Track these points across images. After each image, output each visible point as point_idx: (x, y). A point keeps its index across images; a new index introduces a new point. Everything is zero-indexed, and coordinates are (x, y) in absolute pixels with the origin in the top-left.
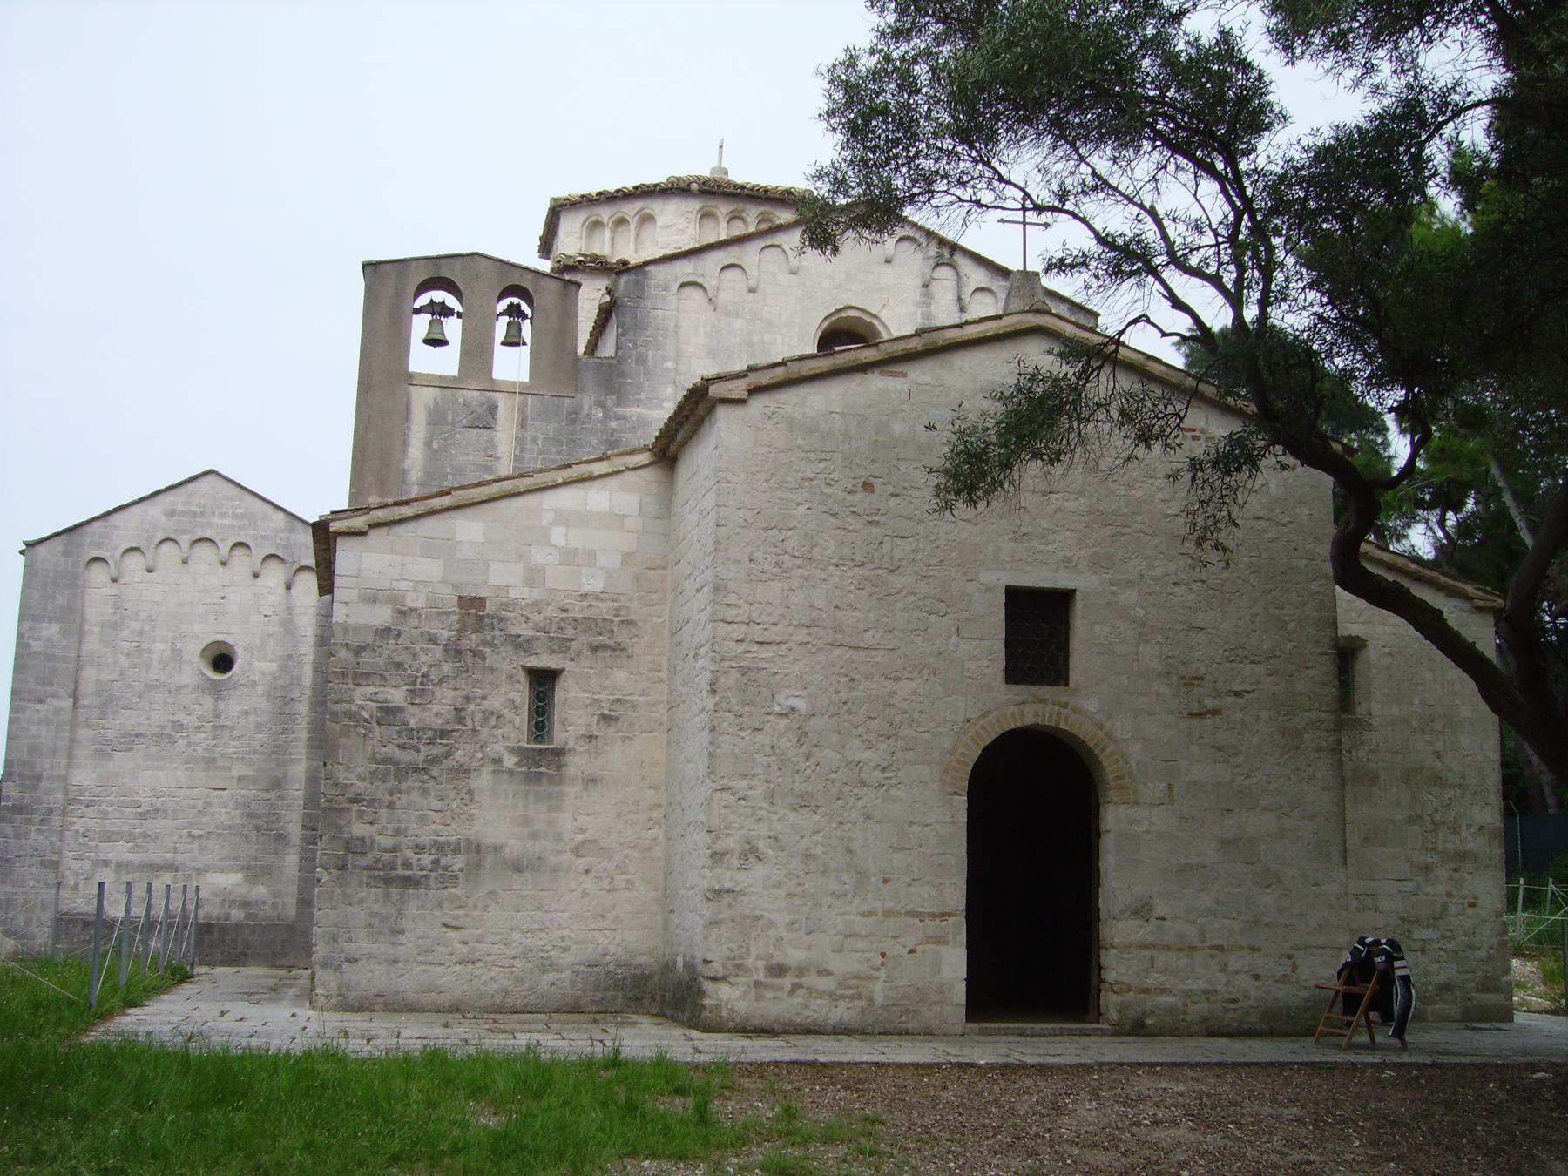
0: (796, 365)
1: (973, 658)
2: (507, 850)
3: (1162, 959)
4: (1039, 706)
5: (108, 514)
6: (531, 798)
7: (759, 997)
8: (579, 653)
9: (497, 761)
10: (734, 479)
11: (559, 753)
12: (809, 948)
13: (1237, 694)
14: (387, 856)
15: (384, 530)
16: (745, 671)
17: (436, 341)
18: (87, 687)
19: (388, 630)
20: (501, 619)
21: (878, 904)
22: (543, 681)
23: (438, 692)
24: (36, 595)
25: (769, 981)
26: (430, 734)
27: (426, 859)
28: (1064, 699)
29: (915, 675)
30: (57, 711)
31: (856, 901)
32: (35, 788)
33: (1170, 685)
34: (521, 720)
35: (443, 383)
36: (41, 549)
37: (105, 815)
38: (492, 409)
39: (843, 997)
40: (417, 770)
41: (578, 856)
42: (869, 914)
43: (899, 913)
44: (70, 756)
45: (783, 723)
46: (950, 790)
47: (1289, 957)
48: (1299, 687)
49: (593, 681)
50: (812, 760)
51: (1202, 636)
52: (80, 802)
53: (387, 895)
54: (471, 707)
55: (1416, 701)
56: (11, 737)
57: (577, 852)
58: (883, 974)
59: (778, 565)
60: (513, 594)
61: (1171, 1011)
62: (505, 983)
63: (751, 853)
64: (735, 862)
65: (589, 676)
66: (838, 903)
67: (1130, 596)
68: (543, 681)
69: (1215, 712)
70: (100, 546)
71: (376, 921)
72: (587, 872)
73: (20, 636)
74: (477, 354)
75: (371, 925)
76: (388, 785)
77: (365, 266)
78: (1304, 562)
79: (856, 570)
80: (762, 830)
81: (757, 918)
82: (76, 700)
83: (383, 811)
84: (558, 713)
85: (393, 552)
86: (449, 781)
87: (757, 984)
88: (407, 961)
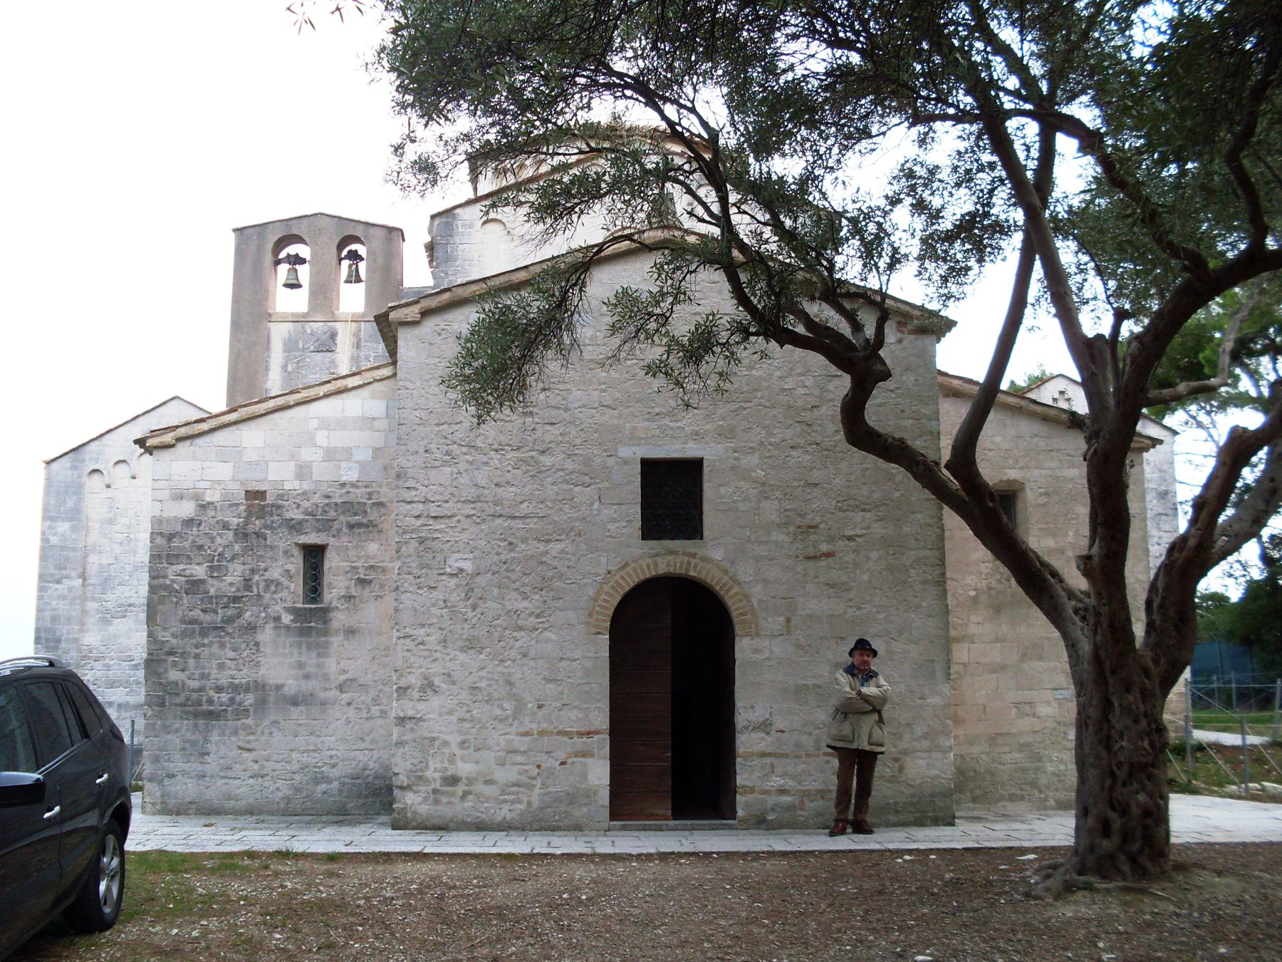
0: (460, 290)
1: (613, 520)
2: (286, 689)
3: (780, 765)
4: (671, 558)
5: (102, 435)
6: (304, 647)
7: (437, 802)
8: (340, 530)
9: (277, 619)
10: (411, 386)
11: (326, 611)
12: (477, 762)
13: (850, 538)
14: (195, 695)
15: (188, 443)
16: (422, 541)
17: (294, 285)
18: (92, 569)
19: (192, 520)
20: (279, 507)
21: (534, 726)
22: (314, 556)
23: (231, 567)
24: (53, 502)
25: (444, 789)
26: (225, 600)
27: (225, 697)
28: (692, 550)
29: (563, 537)
30: (70, 589)
31: (515, 724)
32: (57, 648)
33: (788, 534)
34: (297, 586)
35: (299, 320)
36: (54, 465)
37: (108, 667)
38: (333, 336)
39: (505, 801)
40: (216, 628)
41: (341, 691)
42: (527, 734)
43: (552, 733)
44: (83, 624)
45: (454, 581)
46: (595, 630)
47: (896, 760)
48: (906, 529)
49: (350, 553)
50: (479, 610)
51: (817, 492)
52: (90, 658)
53: (196, 726)
54: (256, 577)
55: (1071, 533)
56: (40, 610)
57: (341, 688)
58: (538, 782)
59: (448, 453)
60: (287, 487)
61: (790, 808)
62: (289, 792)
63: (429, 686)
64: (416, 695)
65: (347, 548)
66: (501, 726)
67: (754, 460)
68: (314, 556)
69: (829, 555)
70: (97, 460)
71: (188, 745)
72: (349, 704)
73: (43, 533)
74: (323, 294)
75: (184, 749)
76: (194, 641)
77: (239, 231)
78: (910, 421)
79: (513, 454)
80: (436, 668)
81: (434, 739)
82: (85, 579)
83: (191, 661)
84: (328, 578)
85: (194, 459)
86: (240, 636)
87: (435, 791)
88: (212, 776)
